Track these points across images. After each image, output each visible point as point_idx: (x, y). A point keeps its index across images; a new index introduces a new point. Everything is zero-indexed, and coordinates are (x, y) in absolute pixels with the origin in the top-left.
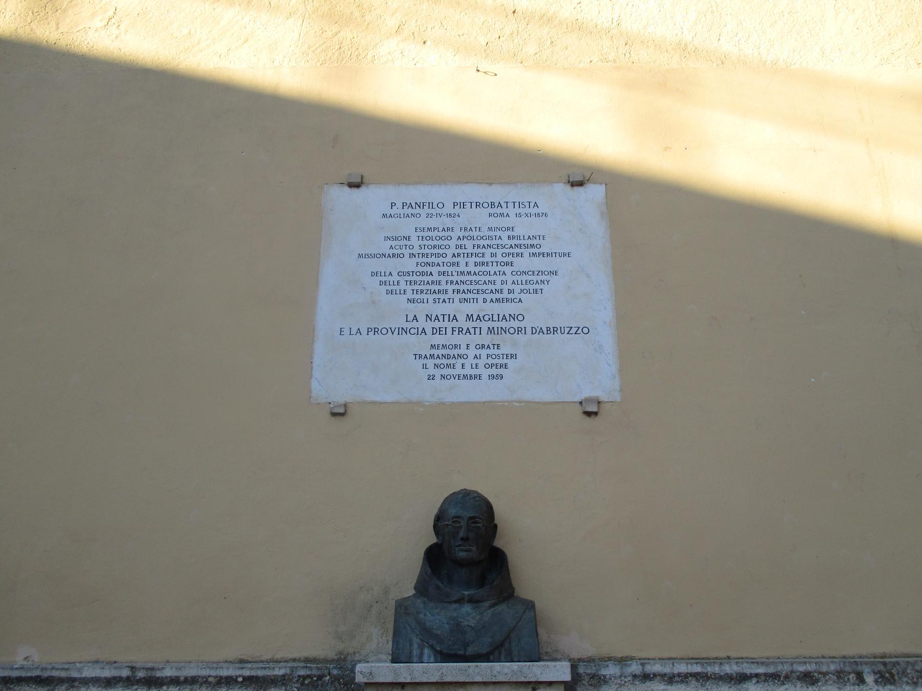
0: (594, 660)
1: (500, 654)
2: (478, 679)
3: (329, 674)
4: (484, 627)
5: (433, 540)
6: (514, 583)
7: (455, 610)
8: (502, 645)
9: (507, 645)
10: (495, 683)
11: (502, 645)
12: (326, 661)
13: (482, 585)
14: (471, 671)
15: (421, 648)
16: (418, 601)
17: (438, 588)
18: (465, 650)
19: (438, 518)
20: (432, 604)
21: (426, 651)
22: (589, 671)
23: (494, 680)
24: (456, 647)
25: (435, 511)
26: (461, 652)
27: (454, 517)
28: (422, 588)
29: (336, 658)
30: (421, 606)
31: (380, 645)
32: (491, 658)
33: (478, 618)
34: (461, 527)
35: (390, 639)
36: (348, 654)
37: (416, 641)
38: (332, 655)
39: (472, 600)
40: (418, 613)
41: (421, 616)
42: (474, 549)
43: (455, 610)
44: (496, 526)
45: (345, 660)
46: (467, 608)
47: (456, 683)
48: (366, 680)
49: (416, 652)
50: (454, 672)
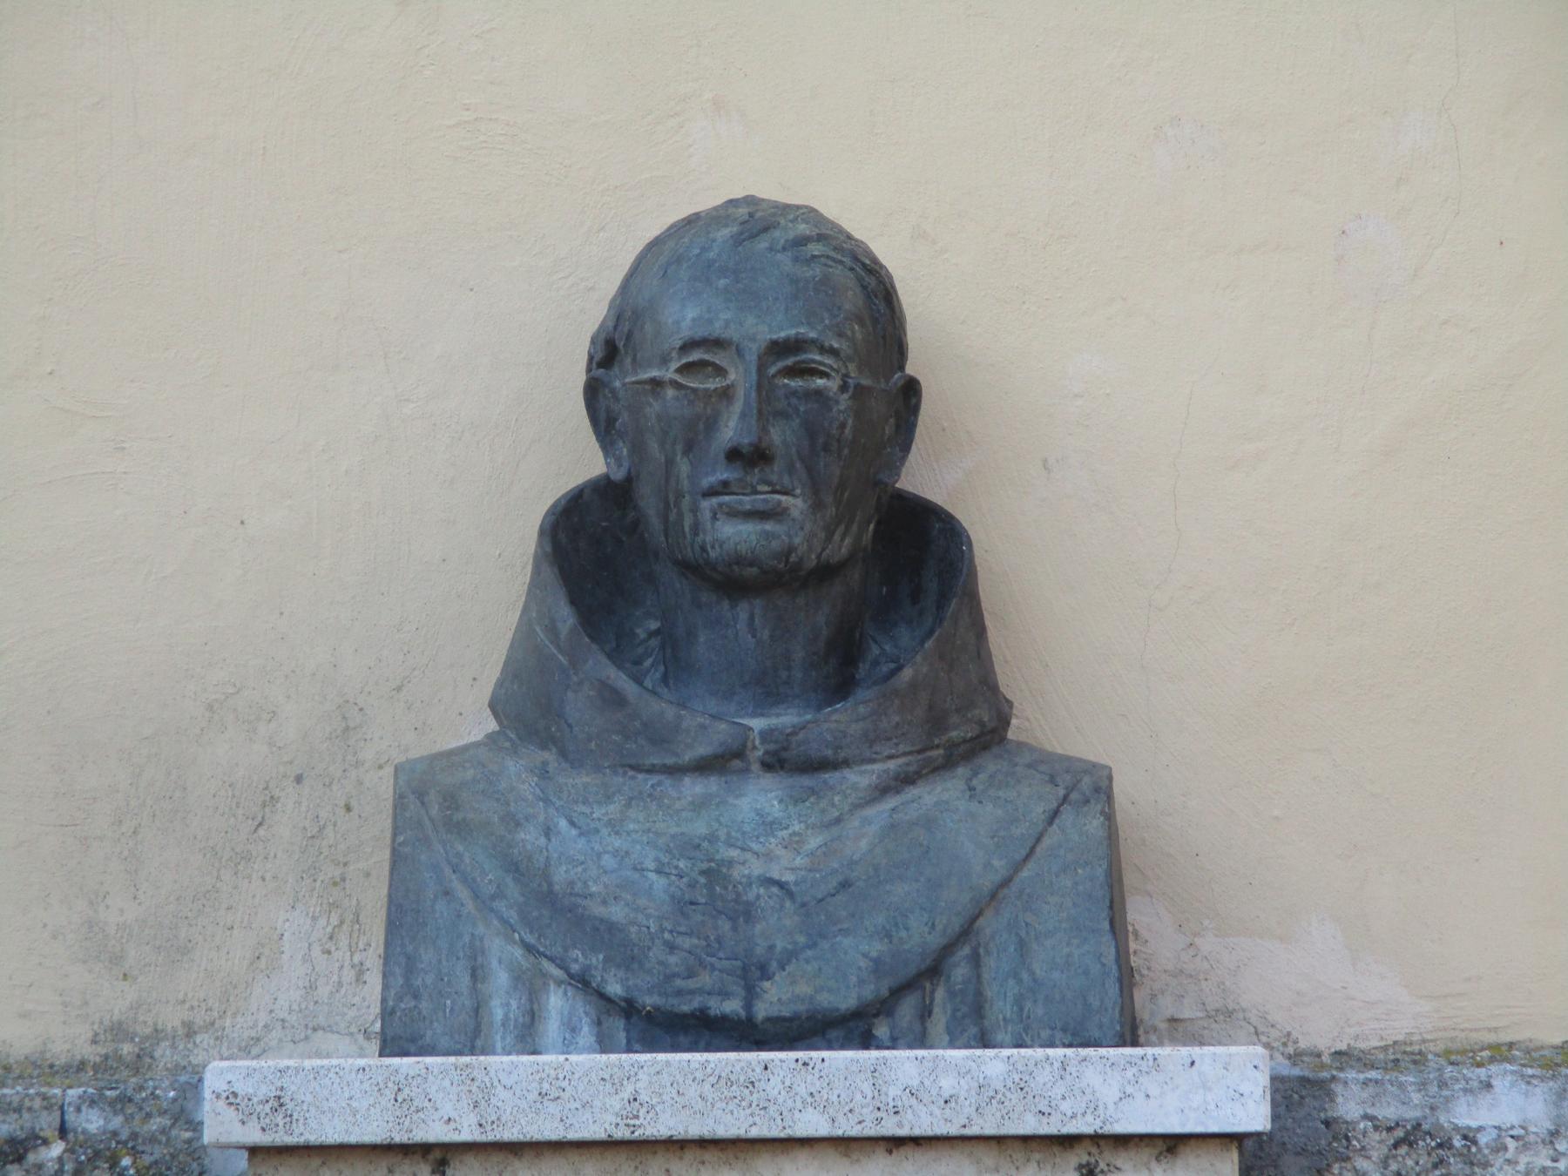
0: (1419, 1060)
1: (925, 1013)
2: (812, 1124)
3: (63, 1131)
4: (845, 885)
5: (585, 461)
6: (1009, 680)
7: (699, 805)
8: (934, 970)
9: (959, 972)
10: (895, 1143)
11: (934, 970)
12: (46, 1069)
13: (840, 686)
14: (774, 1087)
15: (530, 988)
16: (512, 766)
17: (612, 698)
18: (751, 995)
19: (609, 352)
20: (583, 779)
21: (557, 1002)
22: (1388, 1111)
23: (890, 1128)
24: (705, 979)
25: (592, 314)
26: (732, 1006)
27: (688, 346)
28: (531, 708)
29: (92, 1053)
30: (527, 787)
31: (323, 991)
32: (882, 1030)
33: (814, 842)
34: (726, 394)
35: (373, 960)
36: (157, 1034)
37: (503, 956)
38: (70, 1039)
39: (782, 760)
40: (514, 822)
41: (529, 837)
42: (796, 505)
43: (699, 805)
44: (911, 390)
45: (140, 1063)
46: (761, 797)
47: (703, 1143)
48: (255, 1136)
49: (502, 1005)
50: (692, 1092)
